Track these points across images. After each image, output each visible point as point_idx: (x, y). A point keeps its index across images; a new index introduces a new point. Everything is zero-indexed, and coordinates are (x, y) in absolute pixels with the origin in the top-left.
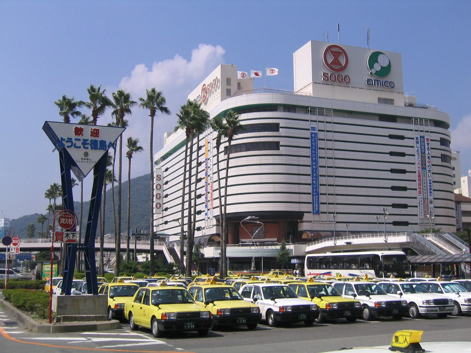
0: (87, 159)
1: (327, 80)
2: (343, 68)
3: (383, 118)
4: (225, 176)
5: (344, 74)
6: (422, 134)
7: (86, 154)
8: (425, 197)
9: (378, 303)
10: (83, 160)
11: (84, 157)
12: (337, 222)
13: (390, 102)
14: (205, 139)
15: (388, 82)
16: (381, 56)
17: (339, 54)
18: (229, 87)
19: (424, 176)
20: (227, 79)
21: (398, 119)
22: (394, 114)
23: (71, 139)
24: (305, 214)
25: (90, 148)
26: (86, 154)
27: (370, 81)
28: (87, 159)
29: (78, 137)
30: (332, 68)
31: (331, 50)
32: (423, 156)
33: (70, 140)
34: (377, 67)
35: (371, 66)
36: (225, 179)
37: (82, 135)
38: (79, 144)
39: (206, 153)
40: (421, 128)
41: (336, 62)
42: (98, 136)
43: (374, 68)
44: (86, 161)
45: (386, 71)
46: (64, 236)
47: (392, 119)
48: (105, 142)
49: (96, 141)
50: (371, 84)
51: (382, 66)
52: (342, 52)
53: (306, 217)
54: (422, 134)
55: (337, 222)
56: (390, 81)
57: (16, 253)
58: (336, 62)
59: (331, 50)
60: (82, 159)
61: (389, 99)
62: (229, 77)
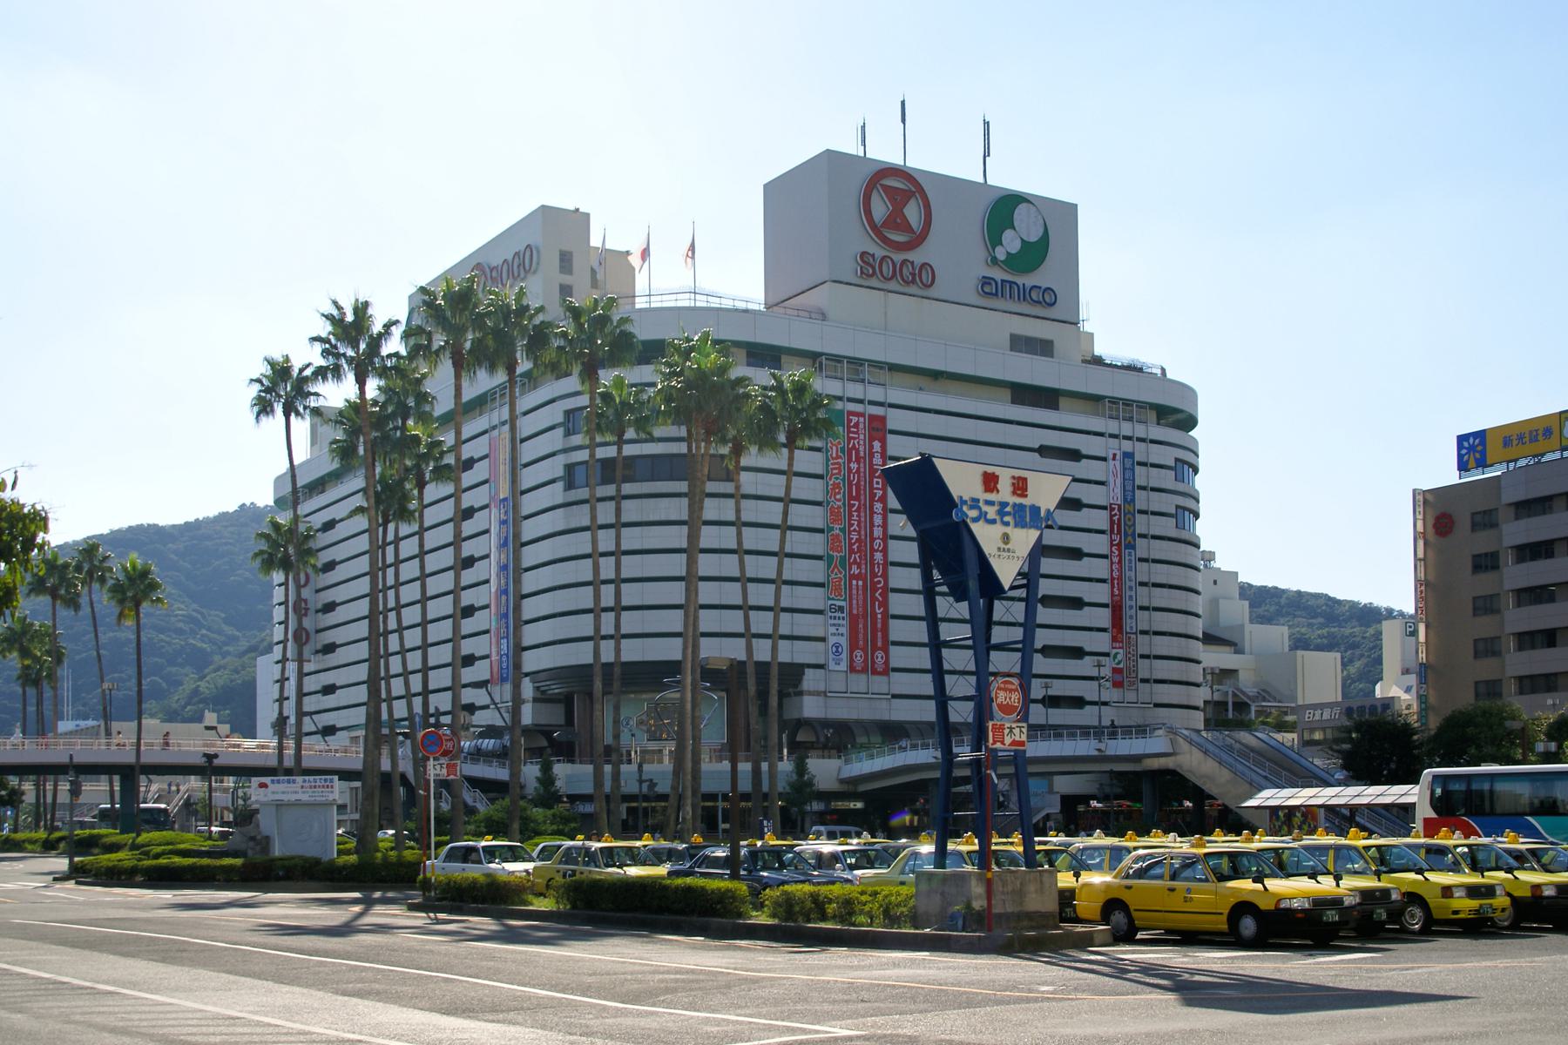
0: (1009, 550)
1: (872, 276)
2: (918, 240)
3: (1026, 394)
4: (416, 551)
5: (917, 256)
6: (1127, 446)
7: (1006, 538)
8: (1131, 628)
9: (1536, 887)
10: (1001, 553)
11: (1003, 546)
12: (894, 696)
13: (1044, 348)
14: (487, 435)
15: (1040, 288)
16: (1023, 206)
17: (906, 196)
18: (567, 279)
19: (1130, 570)
20: (561, 255)
21: (1063, 402)
22: (1056, 386)
23: (978, 500)
24: (806, 670)
25: (1012, 523)
26: (1006, 538)
27: (990, 284)
28: (1009, 550)
29: (991, 497)
30: (886, 241)
31: (882, 182)
32: (1129, 512)
33: (975, 503)
34: (1011, 243)
35: (994, 239)
36: (418, 559)
37: (998, 491)
38: (991, 512)
39: (492, 479)
40: (1126, 428)
41: (896, 220)
42: (1026, 496)
43: (1001, 244)
44: (1005, 554)
45: (1034, 254)
46: (1006, 731)
47: (1046, 397)
48: (1039, 508)
49: (1022, 507)
50: (994, 291)
51: (1025, 239)
52: (913, 189)
53: (811, 680)
54: (1127, 446)
55: (894, 696)
56: (1044, 286)
57: (448, 775)
58: (896, 220)
59: (882, 182)
60: (999, 549)
61: (1041, 340)
62: (565, 248)
